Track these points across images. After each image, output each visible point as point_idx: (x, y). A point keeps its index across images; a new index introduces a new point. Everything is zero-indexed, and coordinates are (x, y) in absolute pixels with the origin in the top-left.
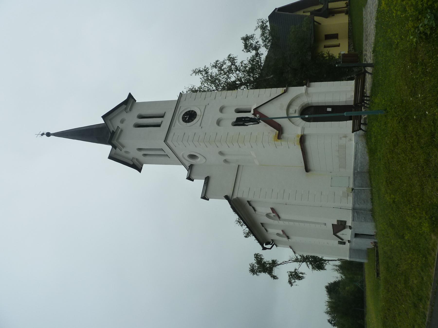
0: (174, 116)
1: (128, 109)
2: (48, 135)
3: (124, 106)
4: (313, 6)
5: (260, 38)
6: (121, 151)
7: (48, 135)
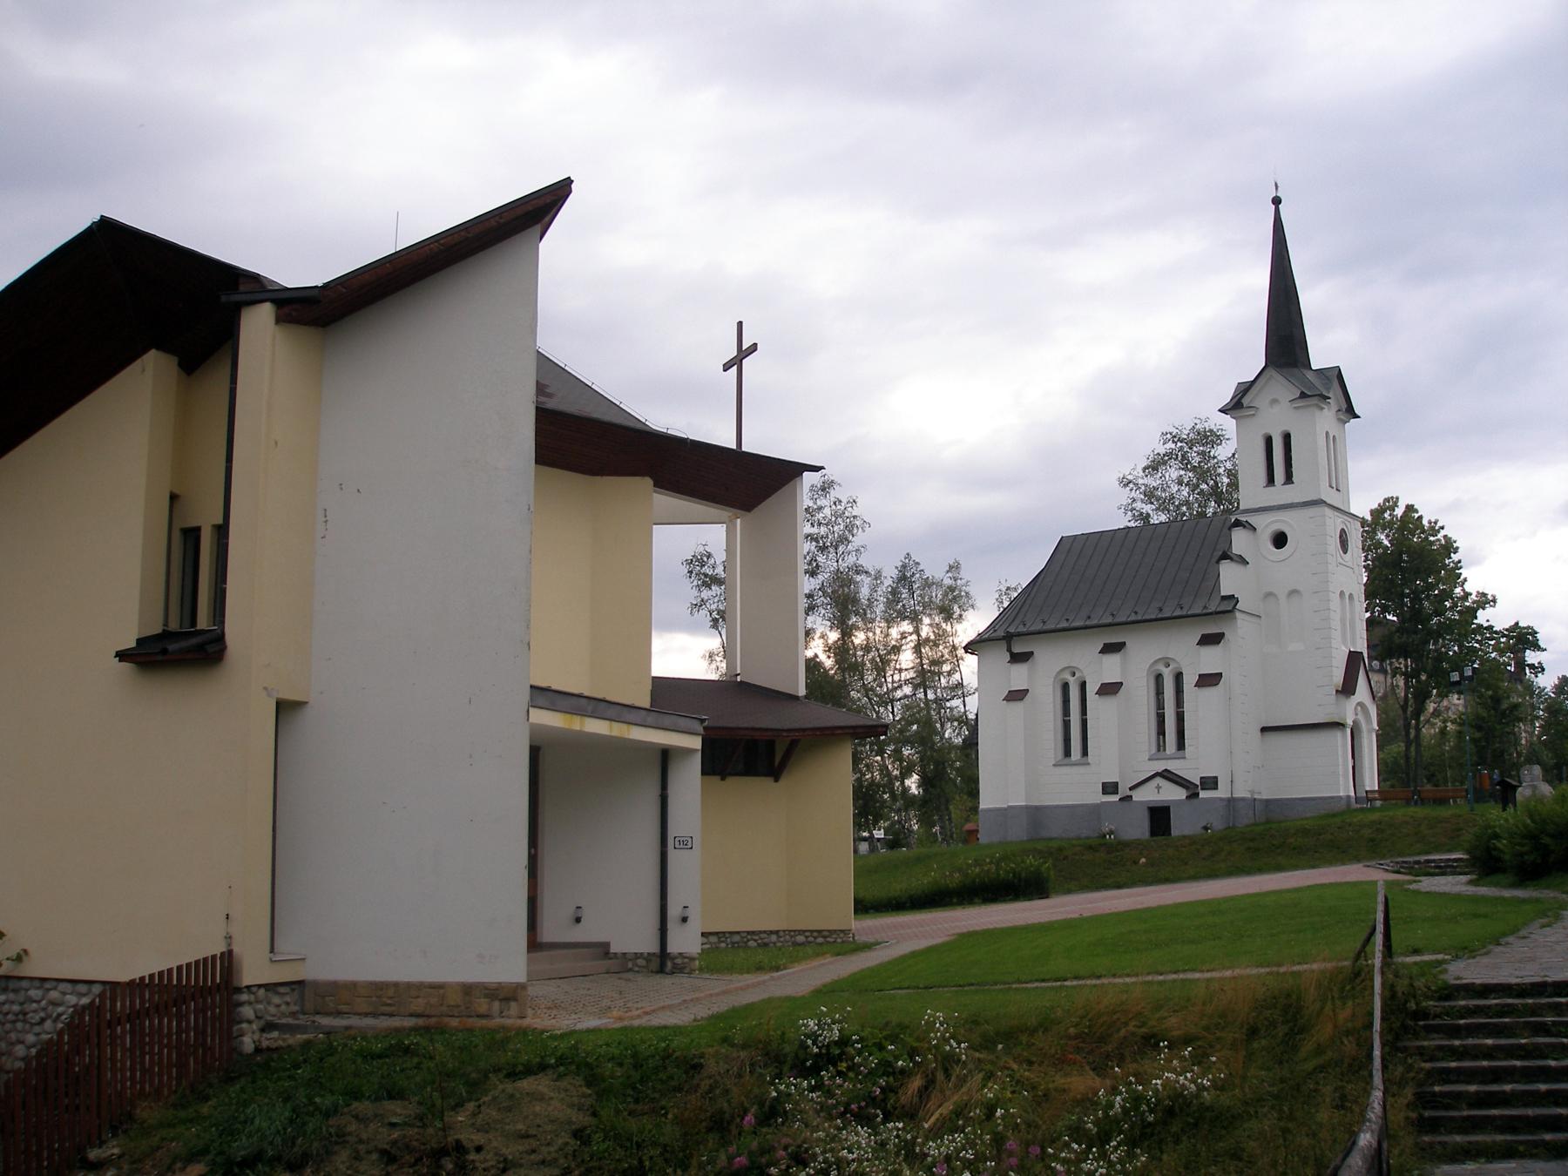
2: (1277, 201)
3: (1344, 406)
7: (1277, 201)
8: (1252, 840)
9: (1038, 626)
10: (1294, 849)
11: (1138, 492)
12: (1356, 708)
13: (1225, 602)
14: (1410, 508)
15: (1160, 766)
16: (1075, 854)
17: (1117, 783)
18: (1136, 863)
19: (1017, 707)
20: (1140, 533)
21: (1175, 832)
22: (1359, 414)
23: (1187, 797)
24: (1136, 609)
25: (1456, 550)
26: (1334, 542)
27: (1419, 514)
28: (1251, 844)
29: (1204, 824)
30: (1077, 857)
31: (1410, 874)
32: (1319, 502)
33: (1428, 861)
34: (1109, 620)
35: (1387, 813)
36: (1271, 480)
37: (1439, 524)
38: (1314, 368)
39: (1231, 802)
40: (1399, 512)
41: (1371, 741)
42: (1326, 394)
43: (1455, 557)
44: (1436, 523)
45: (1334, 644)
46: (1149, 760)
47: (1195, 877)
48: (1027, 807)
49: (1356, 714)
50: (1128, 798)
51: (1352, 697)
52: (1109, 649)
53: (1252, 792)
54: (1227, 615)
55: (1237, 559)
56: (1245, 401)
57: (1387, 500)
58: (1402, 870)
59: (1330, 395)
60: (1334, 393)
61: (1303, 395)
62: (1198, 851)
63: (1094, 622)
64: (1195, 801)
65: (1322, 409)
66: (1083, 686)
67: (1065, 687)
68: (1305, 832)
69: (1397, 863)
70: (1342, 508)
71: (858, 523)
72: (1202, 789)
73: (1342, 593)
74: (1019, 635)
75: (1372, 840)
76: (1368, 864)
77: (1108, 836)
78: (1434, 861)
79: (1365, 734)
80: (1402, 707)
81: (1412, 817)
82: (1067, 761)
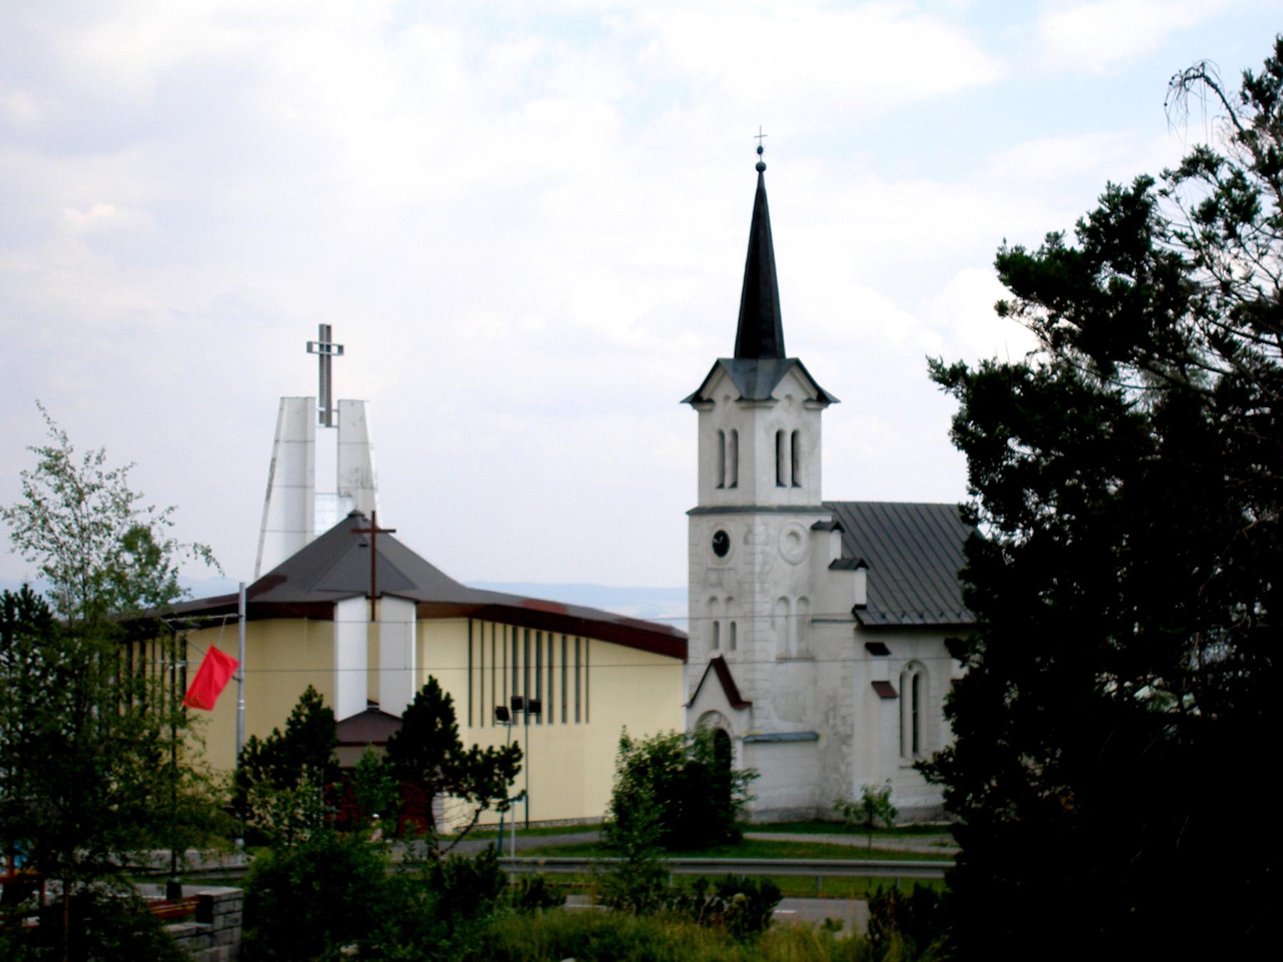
2: (761, 168)
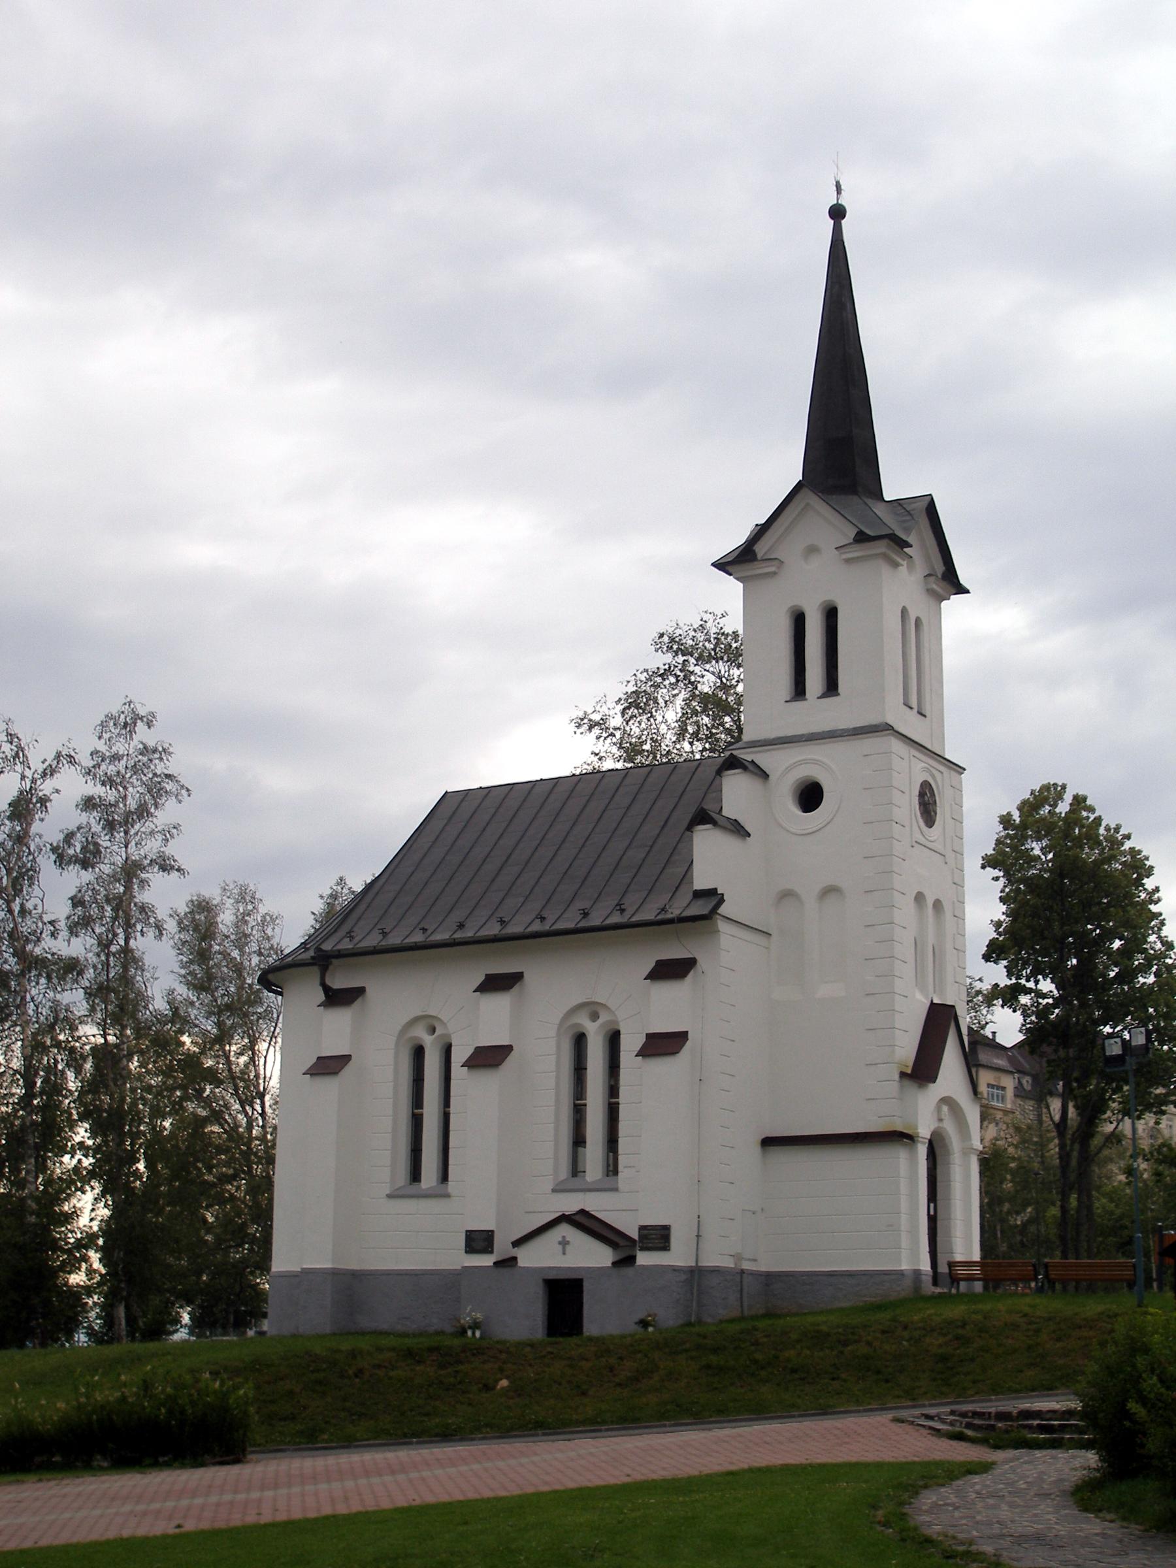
0: (932, 755)
1: (936, 584)
2: (837, 213)
3: (940, 568)
4: (772, 1147)
5: (128, 723)
6: (836, 548)
7: (837, 213)
8: (715, 1350)
9: (373, 941)
10: (794, 1371)
11: (609, 740)
12: (938, 1109)
13: (700, 902)
14: (1079, 802)
15: (571, 1203)
16: (379, 1366)
17: (492, 1231)
18: (488, 1388)
19: (329, 1087)
20: (577, 784)
21: (591, 1327)
22: (968, 587)
23: (613, 1263)
24: (544, 914)
25: (1149, 872)
26: (907, 806)
27: (1096, 814)
28: (713, 1359)
29: (641, 1315)
30: (381, 1373)
31: (984, 1442)
32: (885, 729)
33: (1027, 1414)
34: (493, 929)
35: (980, 1306)
36: (799, 690)
37: (1123, 831)
38: (886, 499)
39: (696, 1275)
40: (1063, 808)
41: (967, 1177)
42: (904, 537)
43: (1149, 883)
44: (1117, 829)
45: (899, 986)
46: (554, 1191)
47: (595, 1424)
48: (335, 1273)
49: (940, 1120)
50: (509, 1262)
51: (932, 1085)
52: (495, 984)
53: (738, 1257)
54: (698, 924)
55: (730, 826)
56: (760, 549)
57: (1046, 788)
58: (969, 1433)
59: (910, 540)
60: (918, 539)
61: (861, 538)
62: (611, 1369)
63: (468, 933)
64: (628, 1271)
65: (896, 565)
66: (447, 1051)
67: (418, 1053)
68: (818, 1338)
69: (964, 1415)
70: (929, 747)
71: (169, 786)
72: (642, 1249)
73: (919, 898)
74: (340, 955)
75: (944, 1358)
76: (903, 1414)
77: (469, 1333)
78: (1038, 1414)
79: (956, 1158)
80: (1057, 1126)
81: (1025, 1315)
82: (414, 1189)
